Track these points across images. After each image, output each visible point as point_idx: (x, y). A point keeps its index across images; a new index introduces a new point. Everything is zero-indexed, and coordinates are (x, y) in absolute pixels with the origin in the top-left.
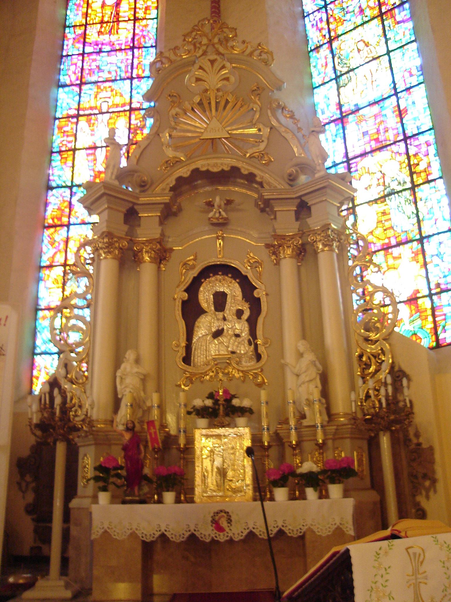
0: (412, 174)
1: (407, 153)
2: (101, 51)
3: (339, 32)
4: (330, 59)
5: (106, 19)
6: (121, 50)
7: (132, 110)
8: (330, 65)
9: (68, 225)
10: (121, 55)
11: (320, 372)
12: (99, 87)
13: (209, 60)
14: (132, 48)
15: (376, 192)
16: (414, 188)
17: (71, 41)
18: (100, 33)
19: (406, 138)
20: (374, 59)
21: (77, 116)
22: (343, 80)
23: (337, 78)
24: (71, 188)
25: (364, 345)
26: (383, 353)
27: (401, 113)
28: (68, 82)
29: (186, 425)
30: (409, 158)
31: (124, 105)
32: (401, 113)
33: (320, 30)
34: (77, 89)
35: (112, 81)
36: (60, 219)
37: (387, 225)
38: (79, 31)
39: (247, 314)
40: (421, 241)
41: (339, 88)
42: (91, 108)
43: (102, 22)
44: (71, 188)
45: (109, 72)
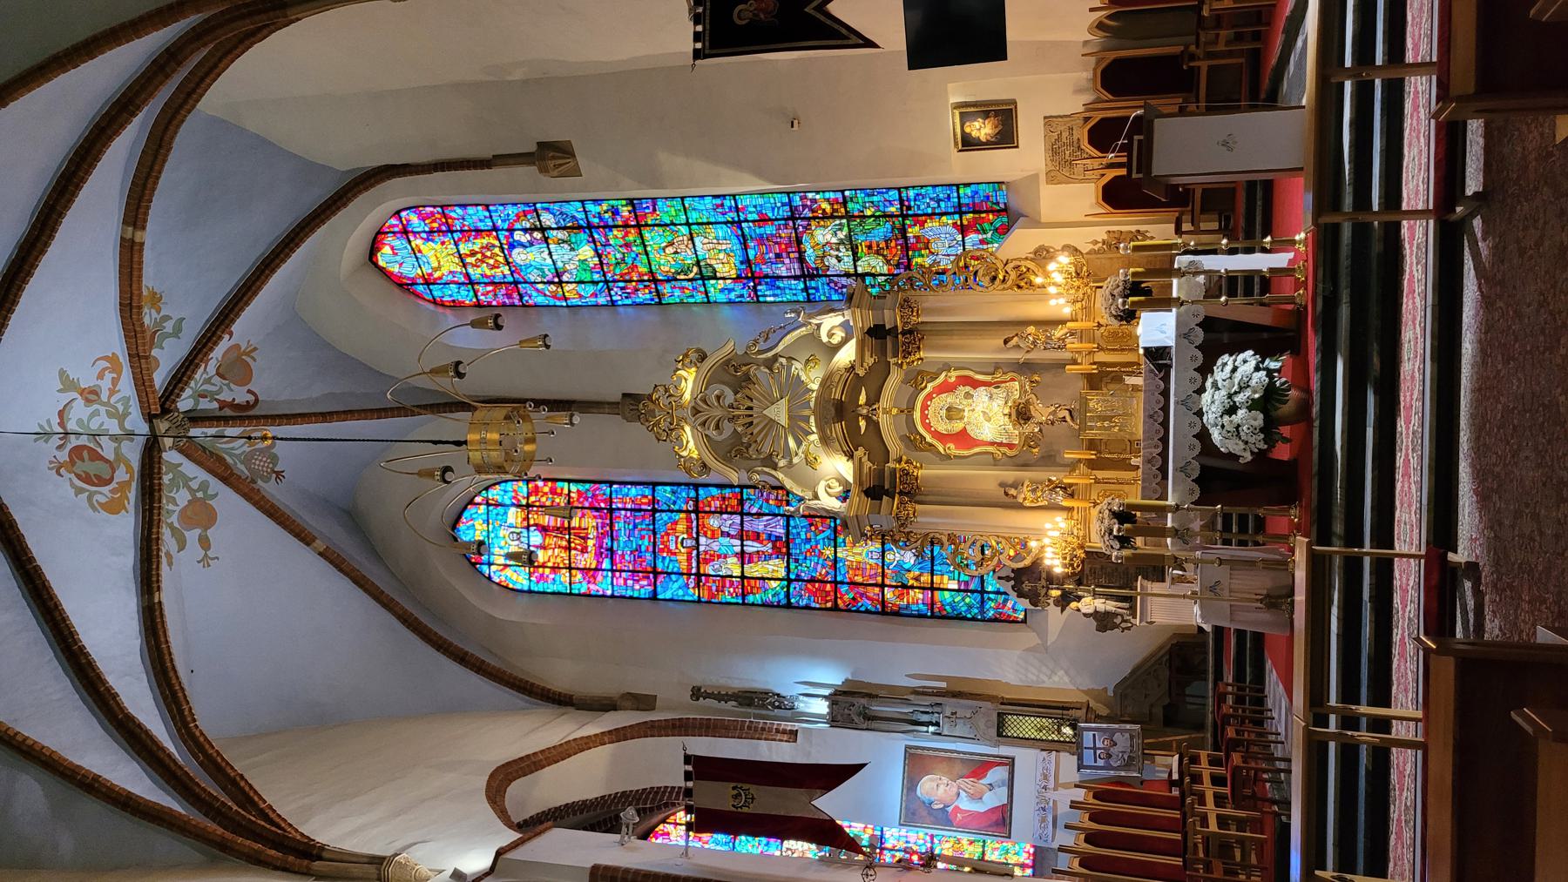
0: (832, 217)
1: (809, 219)
2: (611, 549)
3: (646, 270)
4: (678, 284)
5: (564, 543)
6: (611, 525)
7: (697, 511)
8: (685, 284)
9: (835, 583)
10: (619, 525)
11: (1196, 474)
12: (662, 550)
13: (62, 373)
14: (611, 511)
15: (845, 253)
16: (849, 217)
17: (592, 587)
18: (584, 550)
19: (793, 218)
20: (692, 239)
21: (698, 575)
22: (707, 272)
23: (703, 278)
24: (790, 581)
25: (1009, 283)
26: (1018, 267)
27: (763, 220)
28: (650, 589)
29: (473, 442)
30: (814, 218)
31: (689, 520)
32: (763, 220)
33: (637, 290)
34: (661, 578)
35: (655, 534)
36: (828, 593)
37: (882, 245)
38: (579, 576)
39: (968, 388)
40: (905, 217)
41: (715, 278)
42: (689, 558)
43: (568, 549)
44: (790, 581)
45: (642, 538)
